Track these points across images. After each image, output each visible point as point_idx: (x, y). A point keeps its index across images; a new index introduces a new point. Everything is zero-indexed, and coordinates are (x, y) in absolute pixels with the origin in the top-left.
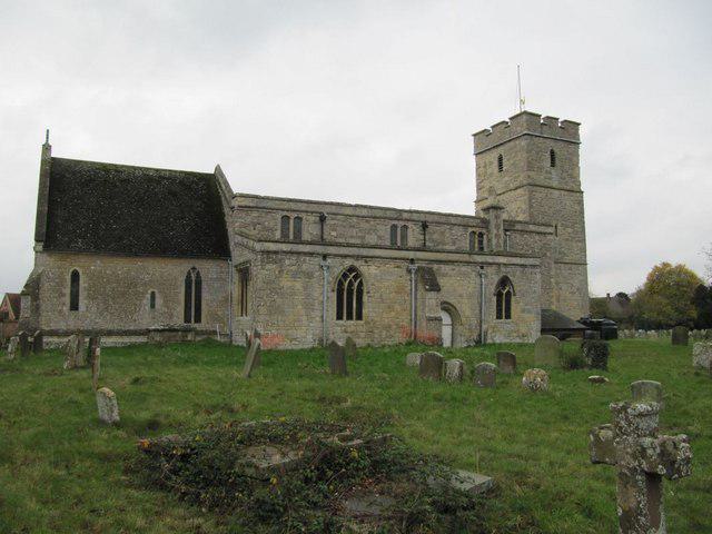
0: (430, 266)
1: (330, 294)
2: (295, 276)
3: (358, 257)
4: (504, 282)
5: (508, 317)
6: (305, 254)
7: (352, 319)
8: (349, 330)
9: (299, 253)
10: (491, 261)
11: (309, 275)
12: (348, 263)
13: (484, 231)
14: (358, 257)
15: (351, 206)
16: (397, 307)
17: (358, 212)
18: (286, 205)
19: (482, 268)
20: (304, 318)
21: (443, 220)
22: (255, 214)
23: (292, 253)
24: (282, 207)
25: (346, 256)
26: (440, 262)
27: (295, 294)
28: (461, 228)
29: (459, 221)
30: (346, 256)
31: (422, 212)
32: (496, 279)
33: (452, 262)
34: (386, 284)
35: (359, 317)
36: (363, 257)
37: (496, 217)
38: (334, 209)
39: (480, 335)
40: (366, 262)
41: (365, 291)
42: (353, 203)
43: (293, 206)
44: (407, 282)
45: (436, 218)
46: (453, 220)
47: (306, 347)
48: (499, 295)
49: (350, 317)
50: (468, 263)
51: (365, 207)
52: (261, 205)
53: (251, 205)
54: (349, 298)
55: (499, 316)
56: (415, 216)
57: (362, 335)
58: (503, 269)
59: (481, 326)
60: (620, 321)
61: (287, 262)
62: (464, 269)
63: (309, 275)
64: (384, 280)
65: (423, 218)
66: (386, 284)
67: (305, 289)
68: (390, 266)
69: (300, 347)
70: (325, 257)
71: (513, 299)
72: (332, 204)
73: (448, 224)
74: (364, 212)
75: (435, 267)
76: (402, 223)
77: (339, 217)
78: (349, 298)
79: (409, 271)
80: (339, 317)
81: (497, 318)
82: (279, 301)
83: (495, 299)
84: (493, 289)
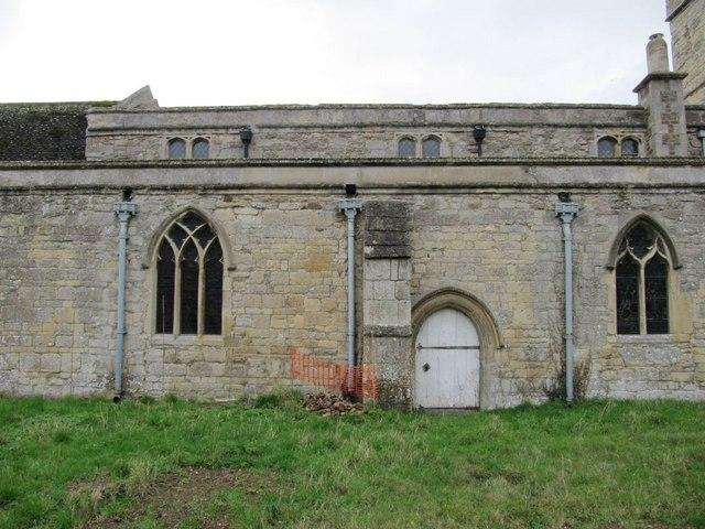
0: (404, 200)
1: (138, 275)
2: (60, 238)
3: (205, 190)
4: (641, 232)
5: (659, 324)
6: (84, 189)
7: (169, 330)
8: (183, 355)
9: (68, 188)
10: (593, 181)
11: (91, 235)
12: (183, 202)
13: (636, 134)
14: (205, 190)
15: (307, 108)
16: (309, 303)
17: (324, 119)
18: (176, 121)
19: (565, 197)
20: (79, 328)
21: (529, 117)
22: (120, 141)
23: (55, 189)
24: (168, 124)
25: (176, 189)
26: (434, 188)
27: (57, 275)
28: (575, 133)
29: (569, 116)
30: (176, 189)
31: (473, 106)
32: (613, 227)
33: (471, 188)
34: (280, 247)
35: (213, 326)
36: (218, 188)
37: (664, 98)
38: (271, 118)
39: (562, 376)
40: (228, 199)
41: (226, 264)
42: (315, 103)
43: (189, 120)
44: (341, 243)
45: (508, 116)
46: (552, 117)
47: (78, 392)
48: (625, 271)
49: (189, 326)
50: (520, 188)
51: (340, 107)
52: (130, 125)
53: (114, 125)
54: (190, 286)
55: (627, 324)
56: (456, 117)
57: (219, 369)
58: (636, 199)
59: (564, 351)
60: (468, 482)
61: (46, 209)
62: (506, 203)
63: (91, 235)
64: (279, 253)
65: (474, 118)
66: (280, 247)
67: (81, 264)
68: (292, 207)
69: (65, 392)
70: (128, 193)
71: (673, 278)
72: (267, 108)
73: (541, 126)
74: (338, 118)
75: (420, 200)
76: (425, 132)
77: (282, 131)
78: (190, 286)
79: (342, 214)
80: (163, 325)
81: (622, 330)
82: (24, 291)
83: (611, 280)
84: (603, 253)
